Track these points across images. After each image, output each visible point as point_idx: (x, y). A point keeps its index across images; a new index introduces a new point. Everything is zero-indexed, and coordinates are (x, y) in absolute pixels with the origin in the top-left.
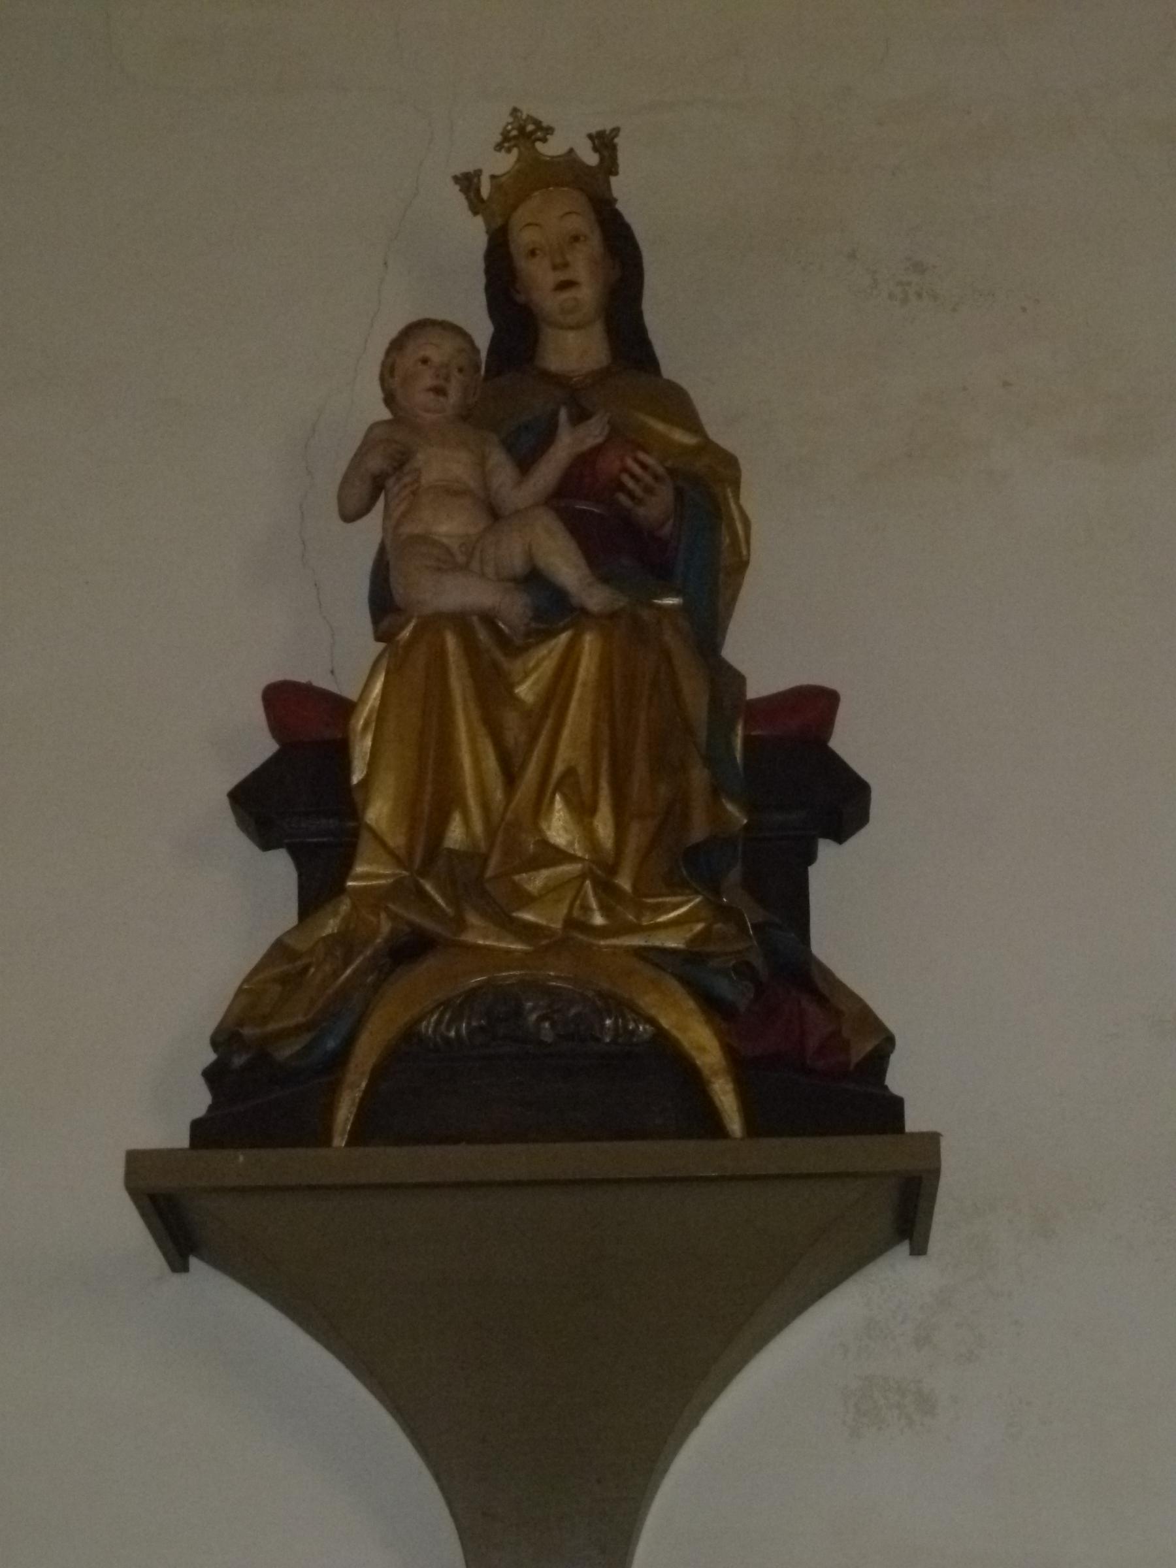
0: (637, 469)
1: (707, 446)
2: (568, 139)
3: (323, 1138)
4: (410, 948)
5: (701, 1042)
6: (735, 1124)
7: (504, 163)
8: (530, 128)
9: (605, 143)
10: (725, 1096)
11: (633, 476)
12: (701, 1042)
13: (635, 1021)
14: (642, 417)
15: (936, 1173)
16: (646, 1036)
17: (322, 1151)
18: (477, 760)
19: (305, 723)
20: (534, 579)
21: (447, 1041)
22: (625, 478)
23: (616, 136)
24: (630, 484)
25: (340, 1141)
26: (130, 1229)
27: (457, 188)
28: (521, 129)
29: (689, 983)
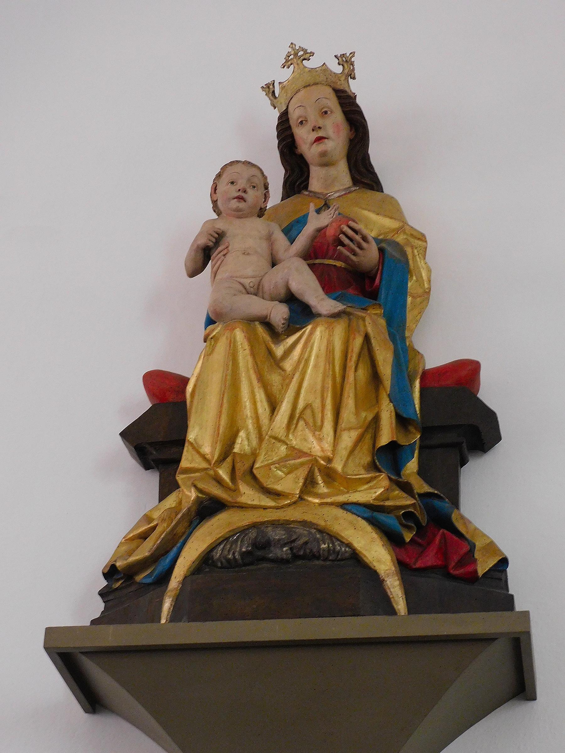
0: (350, 232)
1: (404, 227)
2: (324, 58)
3: (155, 617)
4: (208, 508)
5: (378, 554)
6: (401, 605)
7: (286, 75)
8: (301, 53)
9: (346, 61)
10: (394, 587)
11: (347, 236)
12: (378, 554)
13: (340, 546)
14: (366, 213)
15: (528, 634)
16: (347, 555)
17: (154, 626)
18: (254, 403)
19: (168, 395)
20: (290, 299)
21: (228, 561)
22: (342, 237)
23: (353, 56)
24: (346, 241)
25: (163, 621)
26: (53, 685)
27: (264, 93)
28: (296, 54)
29: (371, 521)
